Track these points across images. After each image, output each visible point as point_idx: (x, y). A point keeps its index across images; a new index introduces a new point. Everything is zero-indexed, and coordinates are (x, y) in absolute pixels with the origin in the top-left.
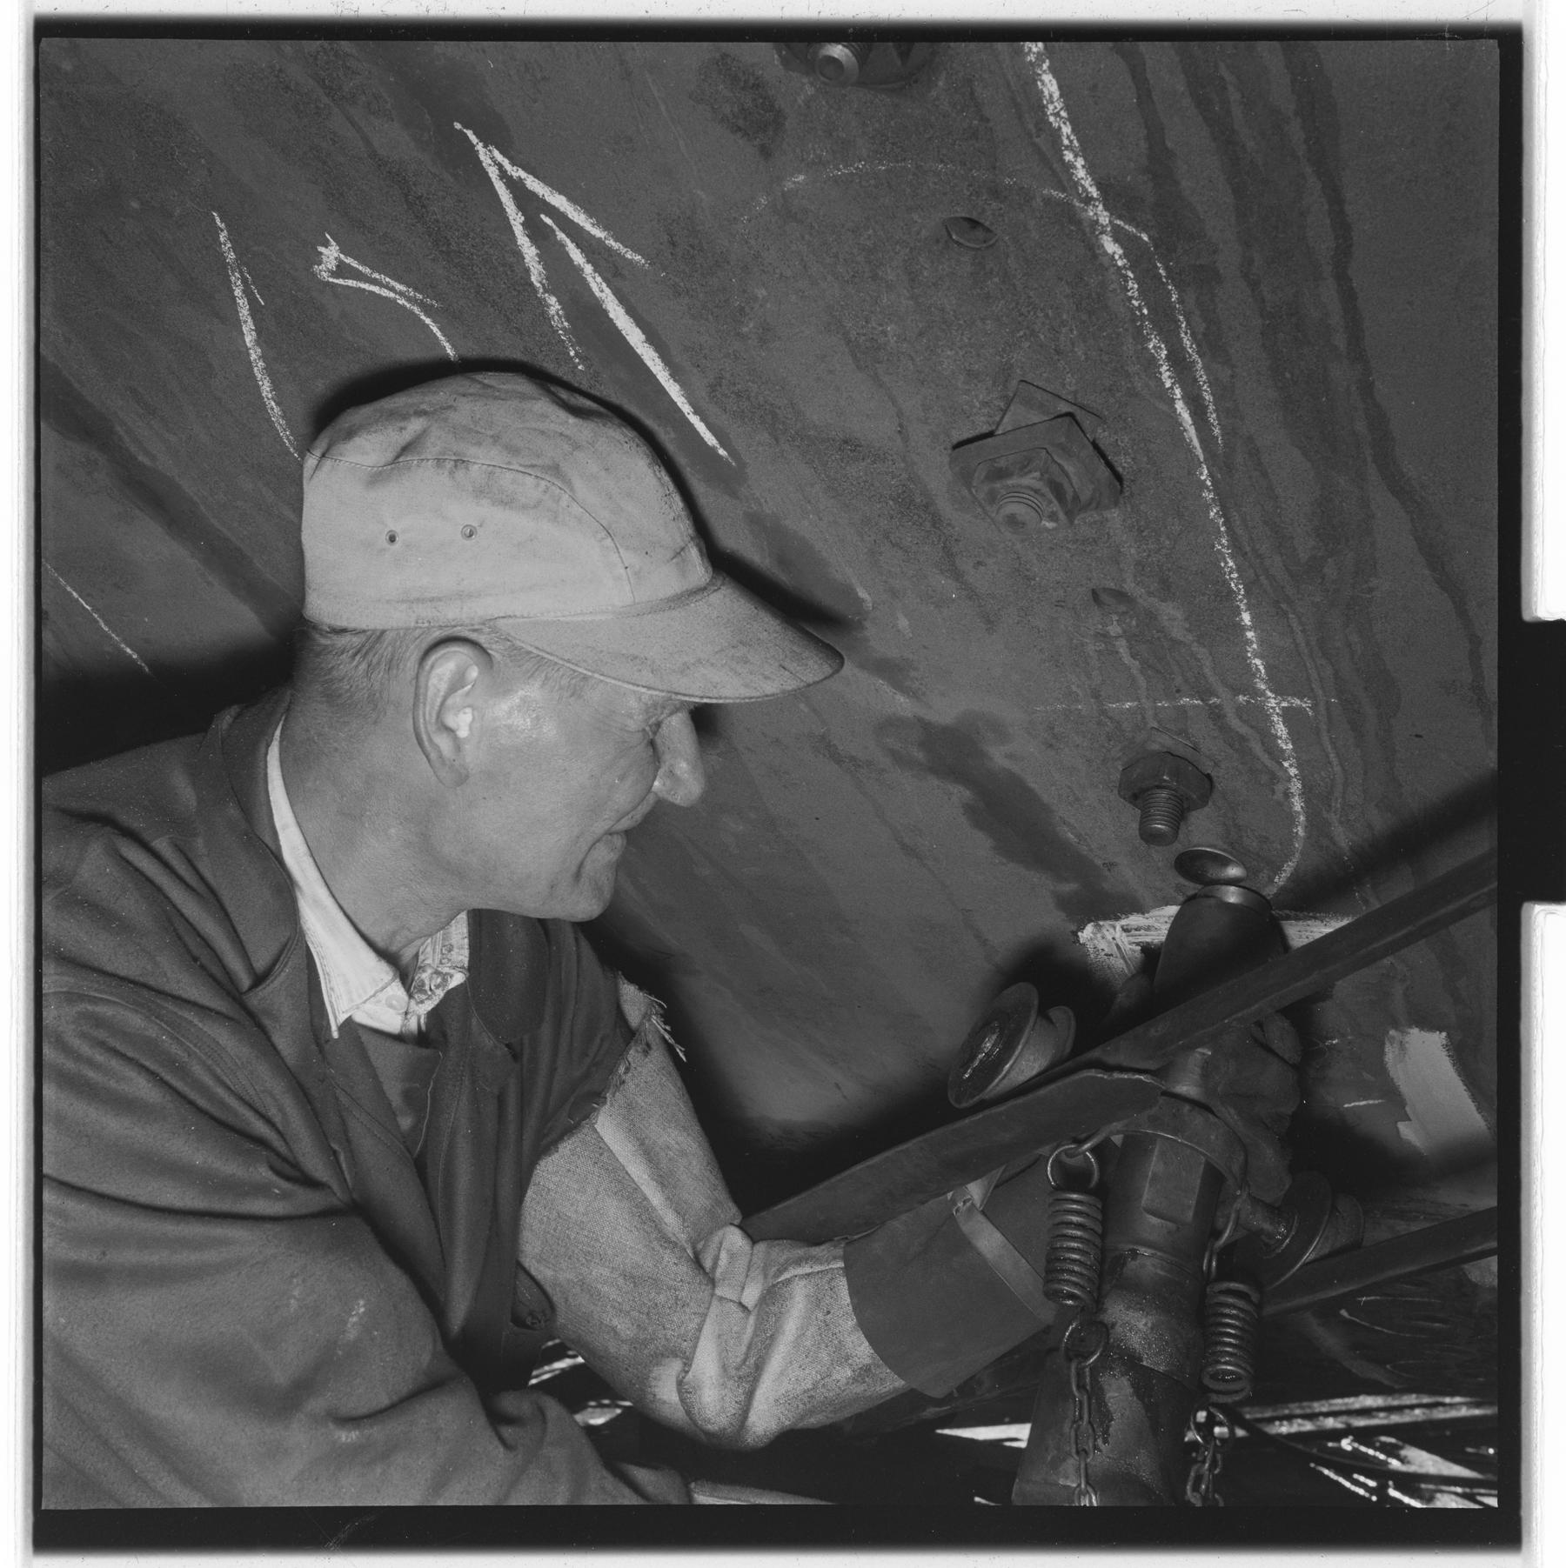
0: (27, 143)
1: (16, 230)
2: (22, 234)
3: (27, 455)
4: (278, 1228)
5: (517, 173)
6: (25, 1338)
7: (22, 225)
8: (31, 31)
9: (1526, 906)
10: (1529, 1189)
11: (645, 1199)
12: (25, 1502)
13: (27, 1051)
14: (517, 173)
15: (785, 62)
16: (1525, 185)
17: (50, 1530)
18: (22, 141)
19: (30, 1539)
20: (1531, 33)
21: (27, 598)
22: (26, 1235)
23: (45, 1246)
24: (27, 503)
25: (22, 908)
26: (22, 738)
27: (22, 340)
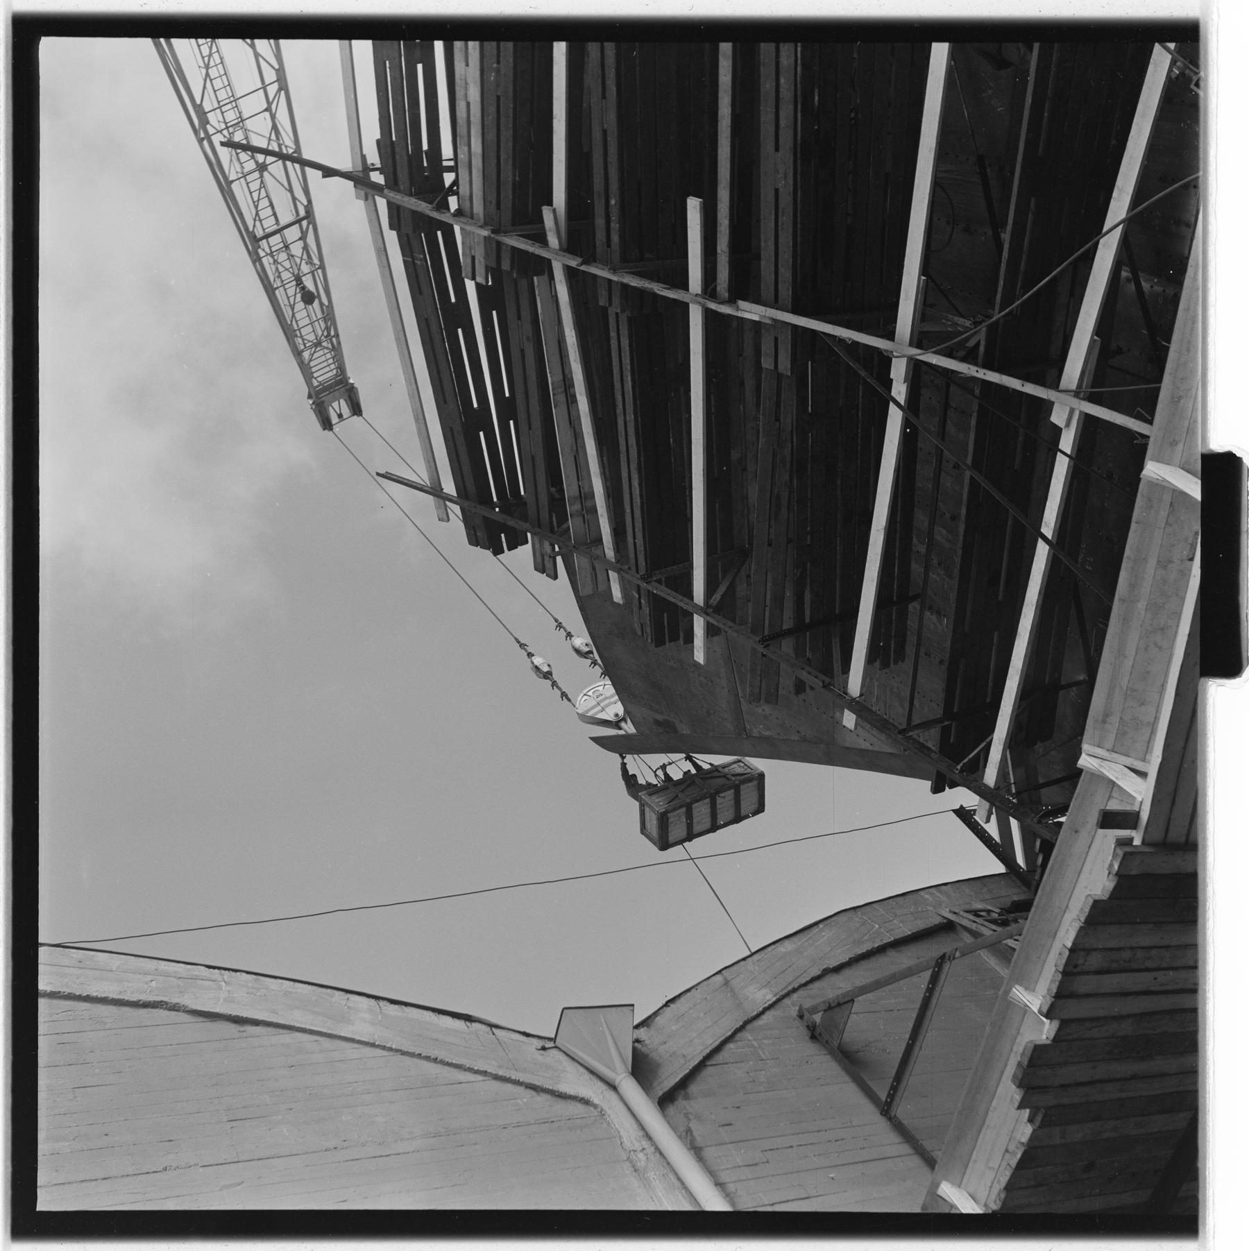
8: (10, 23)
10: (1205, 905)
13: (6, 795)
21: (7, 64)
22: (6, 943)
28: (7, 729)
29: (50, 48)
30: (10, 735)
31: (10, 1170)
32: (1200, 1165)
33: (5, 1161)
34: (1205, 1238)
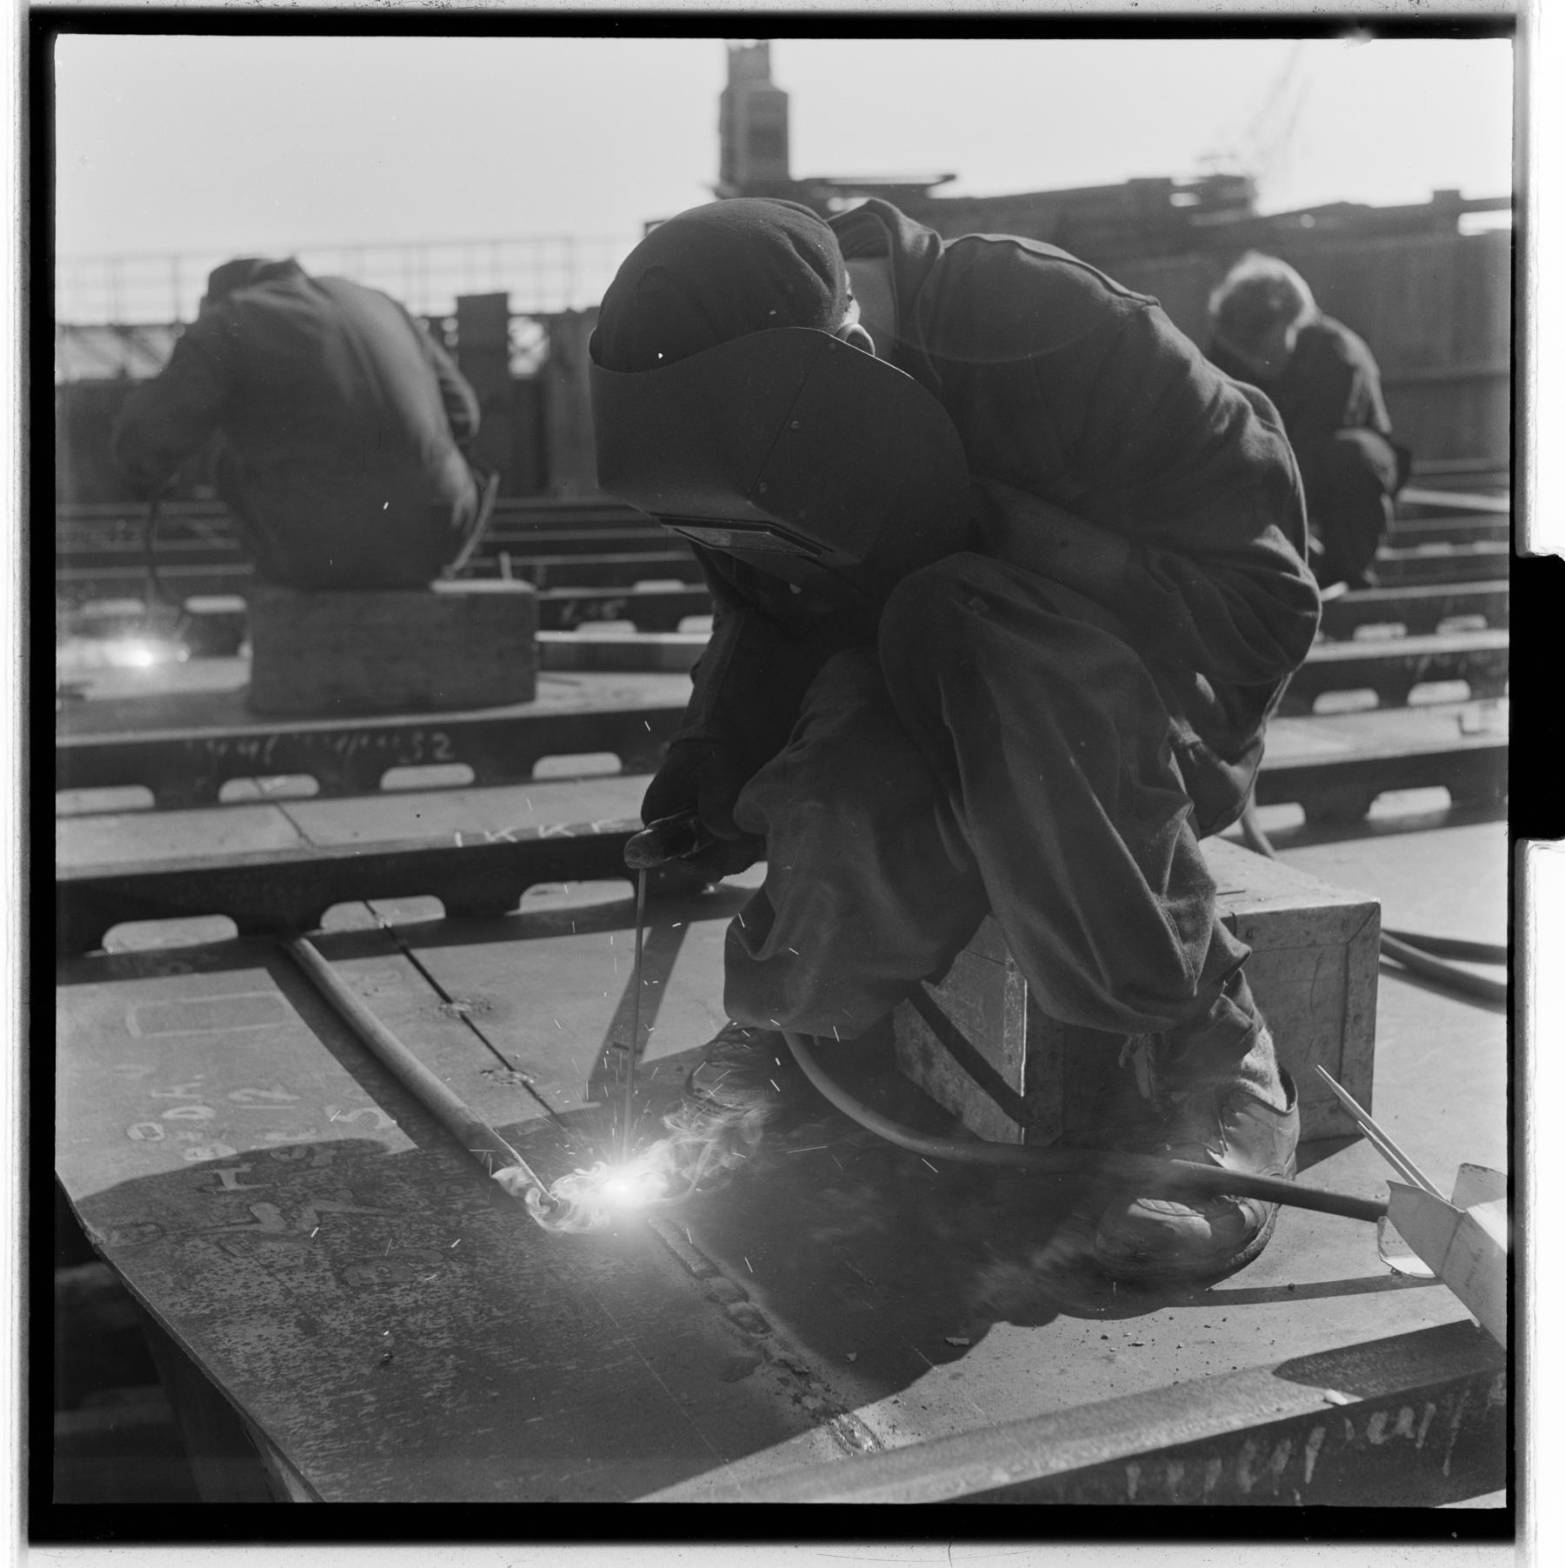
0: (22, 80)
1: (11, 165)
2: (18, 171)
3: (23, 391)
4: (112, 822)
5: (1092, 982)
6: (22, 1274)
7: (18, 160)
8: (27, 19)
9: (1519, 841)
11: (290, 1150)
12: (22, 1437)
14: (1092, 982)
15: (483, 836)
17: (47, 1522)
19: (26, 1536)
23: (62, 529)
24: (22, 439)
25: (18, 844)
26: (18, 673)
27: (18, 177)
28: (23, 1040)
29: (68, 48)
30: (28, 162)
33: (22, 1443)
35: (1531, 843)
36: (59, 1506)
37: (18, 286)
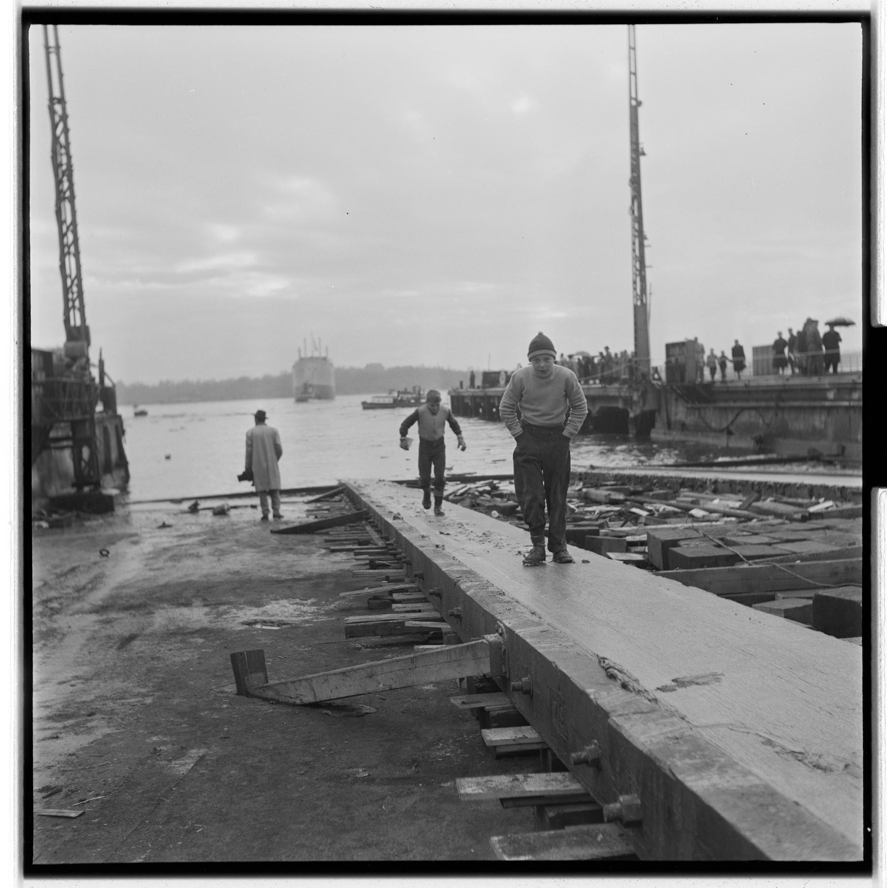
0: (19, 199)
9: (874, 489)
13: (19, 538)
16: (873, 725)
18: (16, 508)
20: (875, 20)
29: (860, 857)
31: (22, 841)
32: (874, 858)
33: (19, 835)
34: (876, 877)
35: (881, 491)
36: (36, 866)
37: (16, 174)
